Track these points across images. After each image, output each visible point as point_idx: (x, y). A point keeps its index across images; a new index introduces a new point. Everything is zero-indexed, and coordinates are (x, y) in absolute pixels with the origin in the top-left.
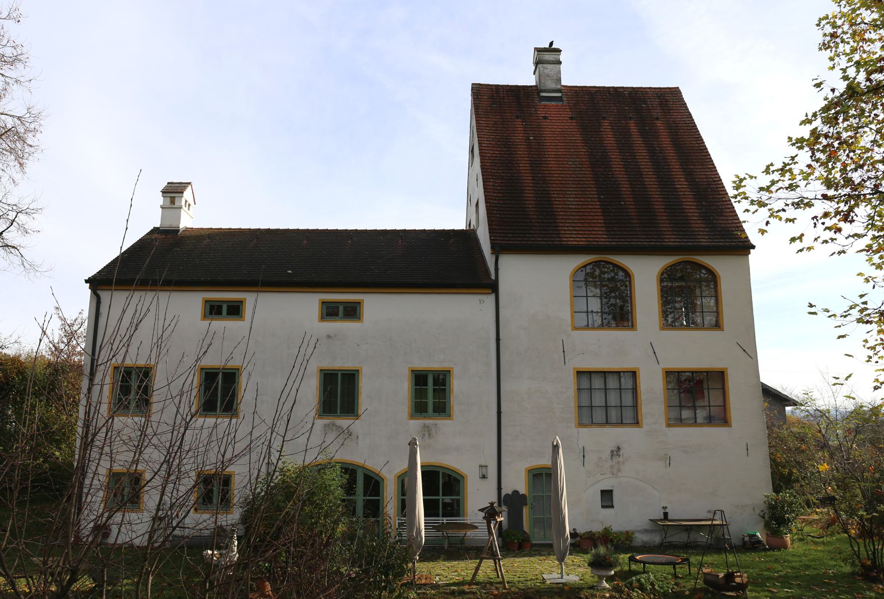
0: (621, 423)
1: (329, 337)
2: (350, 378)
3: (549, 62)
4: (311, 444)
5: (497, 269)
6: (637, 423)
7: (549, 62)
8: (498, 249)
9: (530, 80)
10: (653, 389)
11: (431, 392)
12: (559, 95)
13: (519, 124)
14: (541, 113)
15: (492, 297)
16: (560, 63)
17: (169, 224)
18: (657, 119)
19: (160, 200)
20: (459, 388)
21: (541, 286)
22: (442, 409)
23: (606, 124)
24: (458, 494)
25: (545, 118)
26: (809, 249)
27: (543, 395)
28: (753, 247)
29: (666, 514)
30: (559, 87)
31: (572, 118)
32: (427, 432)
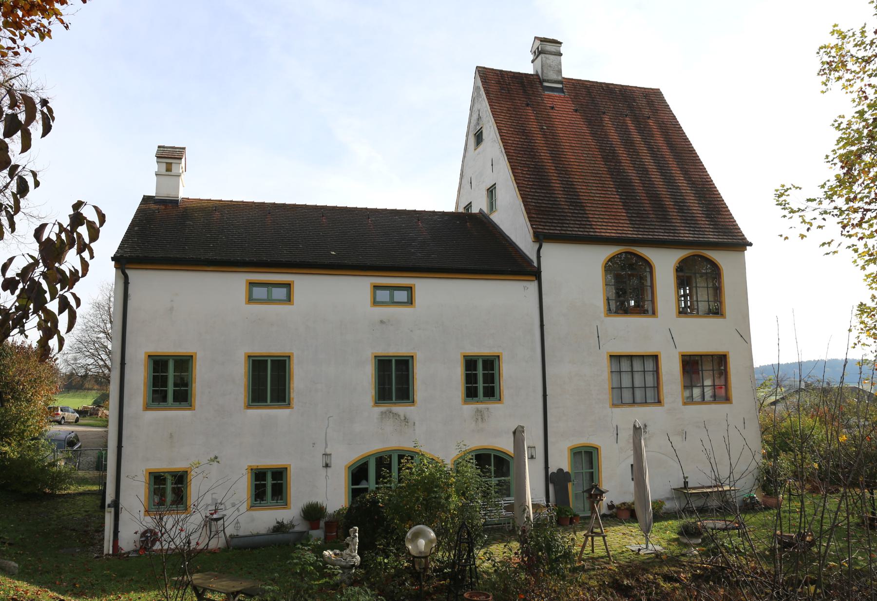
0: (645, 403)
1: (382, 322)
2: (491, 363)
3: (551, 53)
4: (375, 431)
5: (539, 257)
6: (659, 402)
7: (551, 53)
8: (540, 238)
9: (528, 68)
10: (671, 369)
11: (481, 378)
12: (560, 86)
13: (529, 110)
14: (548, 103)
15: (535, 284)
16: (561, 55)
17: (166, 193)
18: (649, 118)
19: (153, 165)
20: (507, 372)
21: (576, 272)
22: (491, 393)
23: (606, 118)
24: (398, 398)
25: (552, 108)
26: (835, 252)
27: (581, 375)
28: (751, 244)
29: (686, 483)
30: (560, 78)
31: (576, 111)
32: (480, 416)
